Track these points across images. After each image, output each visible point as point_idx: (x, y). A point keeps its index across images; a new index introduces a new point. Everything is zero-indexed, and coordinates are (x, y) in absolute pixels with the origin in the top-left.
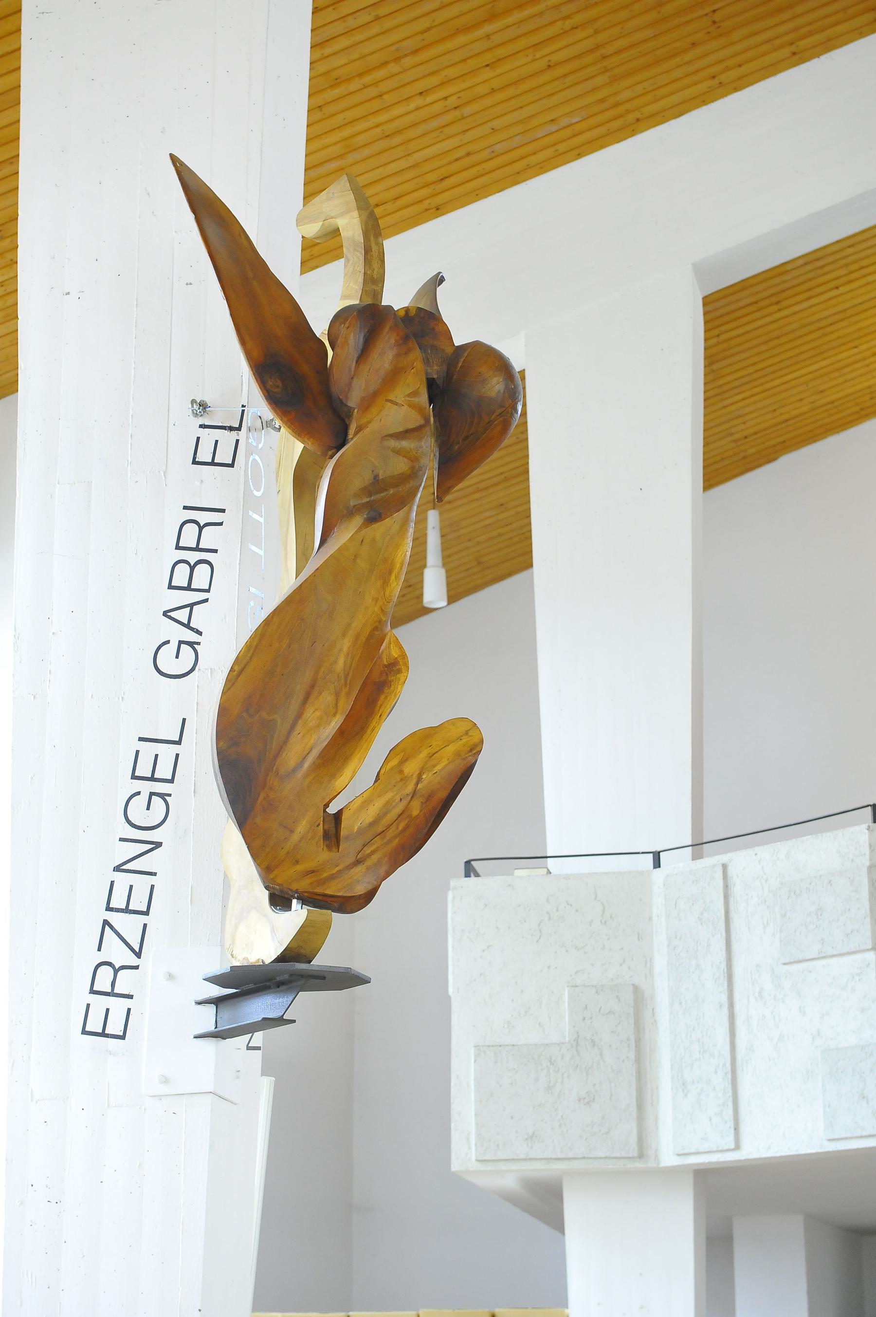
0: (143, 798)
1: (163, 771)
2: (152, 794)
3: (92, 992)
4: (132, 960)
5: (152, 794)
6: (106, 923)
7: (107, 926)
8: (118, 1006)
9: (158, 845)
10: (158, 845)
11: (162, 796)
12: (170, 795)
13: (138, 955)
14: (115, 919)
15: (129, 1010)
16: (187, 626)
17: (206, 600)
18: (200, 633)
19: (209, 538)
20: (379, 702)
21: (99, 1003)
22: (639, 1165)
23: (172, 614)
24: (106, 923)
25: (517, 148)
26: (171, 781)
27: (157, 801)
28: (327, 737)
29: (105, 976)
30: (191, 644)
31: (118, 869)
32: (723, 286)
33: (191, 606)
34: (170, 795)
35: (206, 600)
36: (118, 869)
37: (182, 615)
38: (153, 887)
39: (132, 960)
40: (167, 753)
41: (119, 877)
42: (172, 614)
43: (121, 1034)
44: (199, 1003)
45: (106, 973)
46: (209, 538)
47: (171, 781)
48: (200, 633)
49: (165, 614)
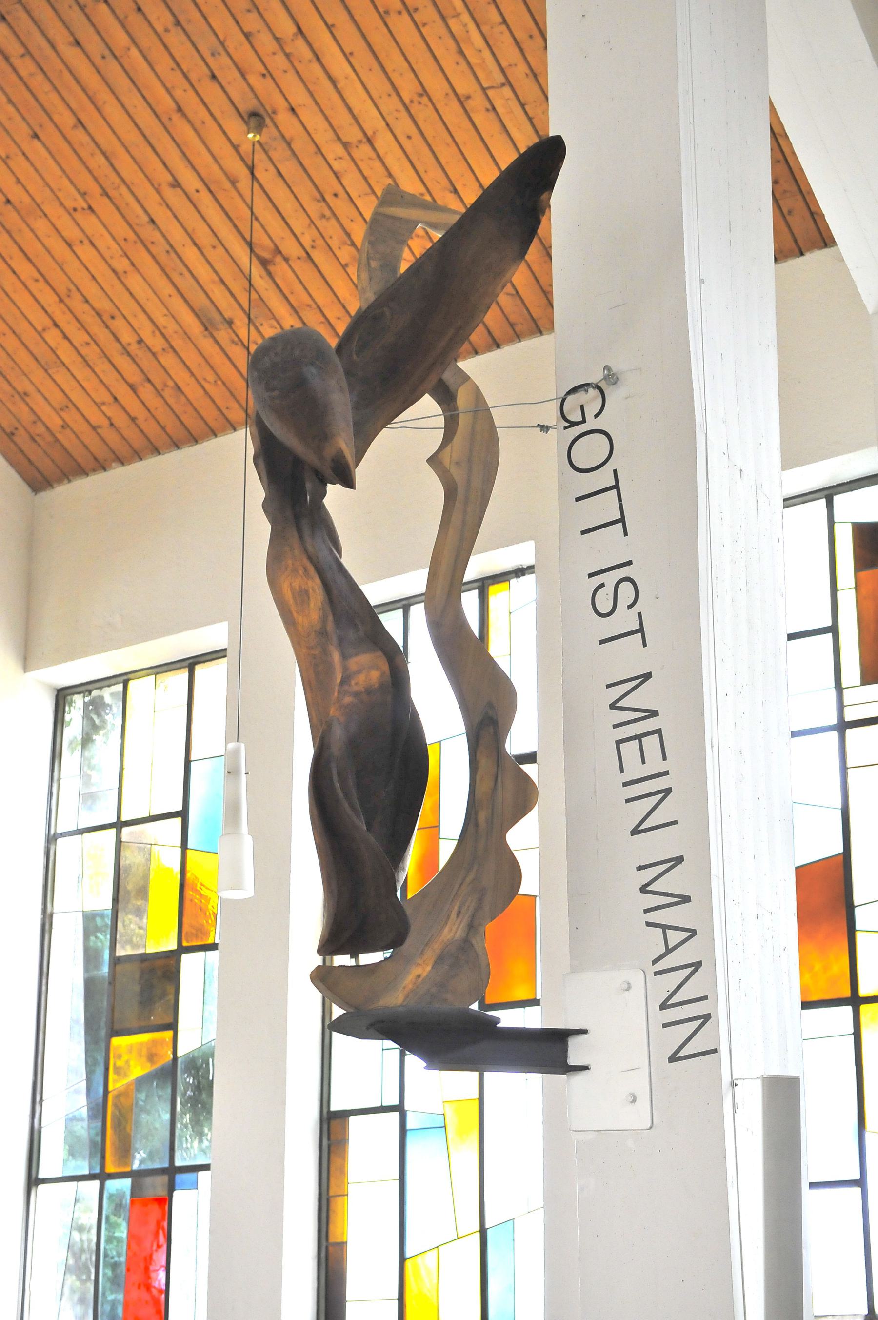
1: (630, 750)
2: (584, 421)
5: (584, 421)
11: (573, 424)
12: (565, 428)
16: (665, 928)
17: (655, 962)
18: (648, 924)
22: (125, 677)
26: (618, 743)
27: (576, 417)
32: (186, 706)
33: (669, 951)
34: (565, 428)
35: (655, 962)
37: (674, 937)
44: (585, 1032)
47: (618, 743)
48: (648, 924)
49: (694, 933)
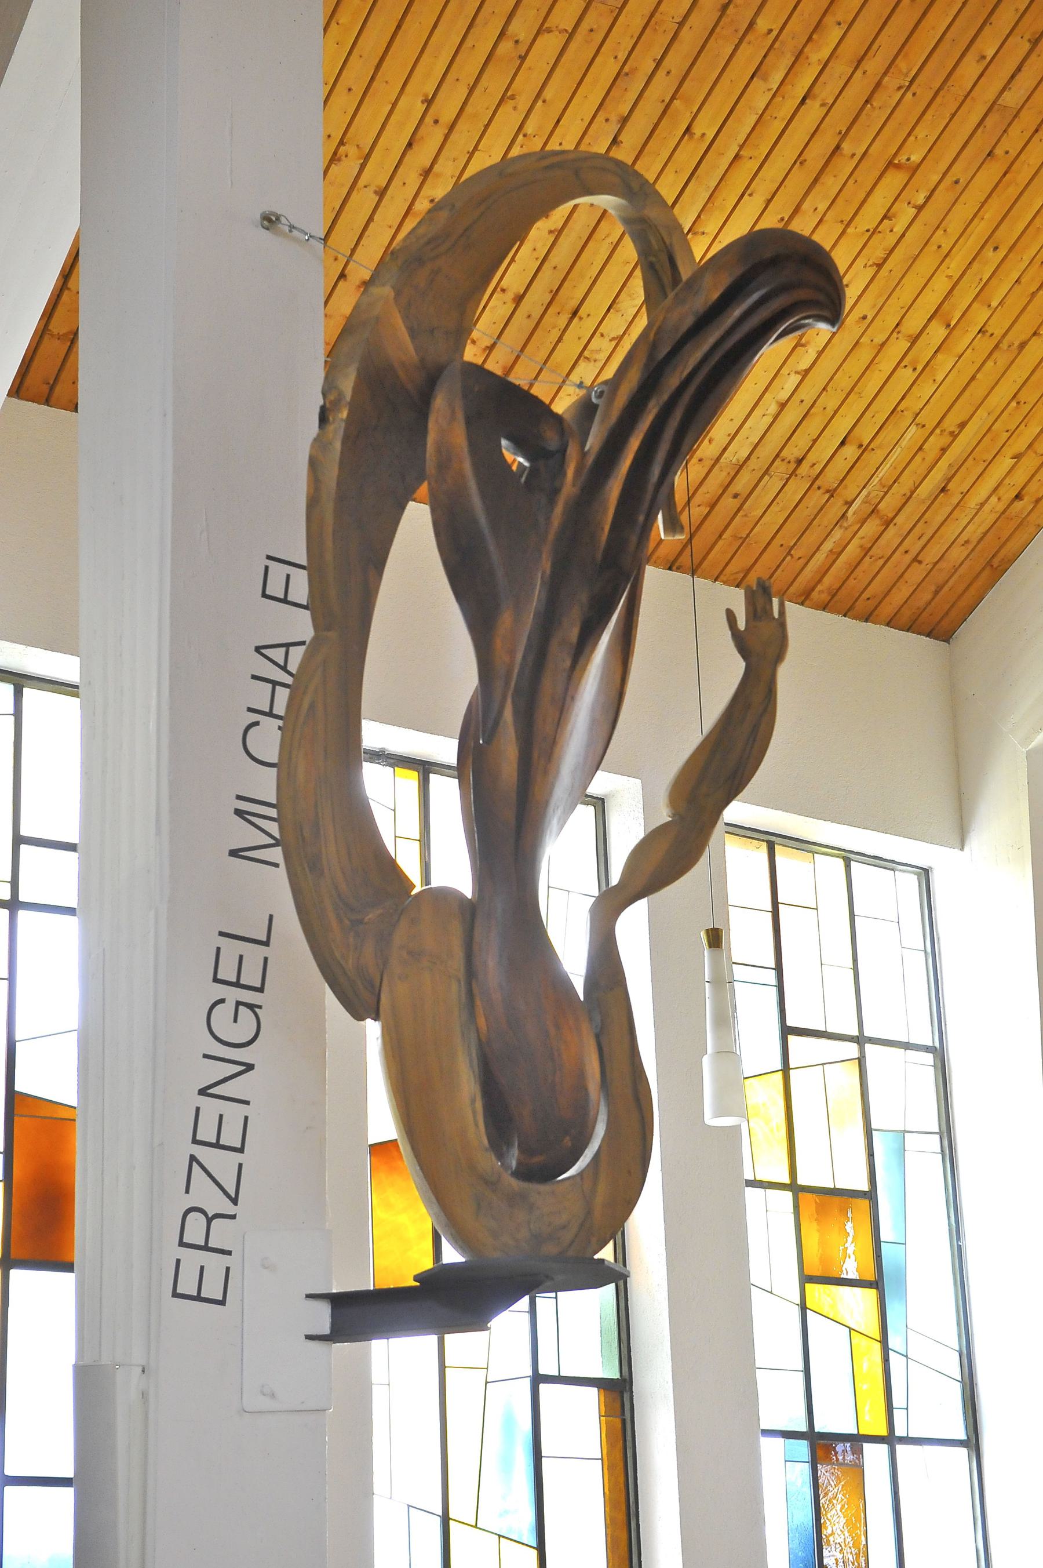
0: (229, 1007)
1: (251, 978)
3: (182, 1244)
4: (228, 1208)
5: (238, 1003)
6: (193, 1158)
7: (194, 1164)
8: (214, 1264)
9: (250, 1067)
10: (250, 1067)
11: (251, 1007)
12: (260, 1007)
13: (235, 1201)
14: (203, 1153)
15: (228, 1269)
19: (221, 1234)
20: (460, 416)
21: (192, 1260)
23: (263, 651)
24: (193, 1158)
25: (999, 380)
26: (261, 990)
28: (473, 1101)
29: (195, 1233)
30: (251, 1007)
31: (203, 1092)
34: (260, 1007)
36: (203, 1092)
37: (278, 655)
38: (240, 1166)
39: (228, 1208)
40: (254, 955)
41: (204, 1102)
42: (263, 651)
43: (259, 986)
45: (196, 1222)
46: (221, 1234)
49: (258, 649)
